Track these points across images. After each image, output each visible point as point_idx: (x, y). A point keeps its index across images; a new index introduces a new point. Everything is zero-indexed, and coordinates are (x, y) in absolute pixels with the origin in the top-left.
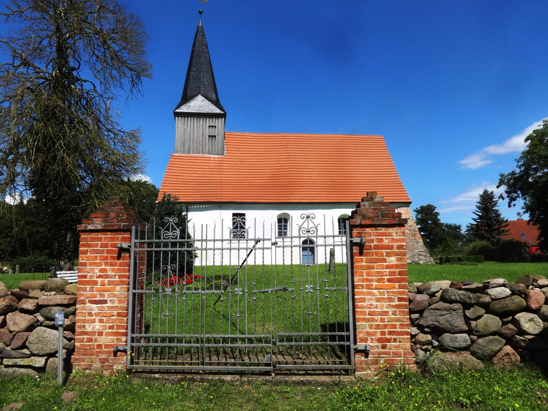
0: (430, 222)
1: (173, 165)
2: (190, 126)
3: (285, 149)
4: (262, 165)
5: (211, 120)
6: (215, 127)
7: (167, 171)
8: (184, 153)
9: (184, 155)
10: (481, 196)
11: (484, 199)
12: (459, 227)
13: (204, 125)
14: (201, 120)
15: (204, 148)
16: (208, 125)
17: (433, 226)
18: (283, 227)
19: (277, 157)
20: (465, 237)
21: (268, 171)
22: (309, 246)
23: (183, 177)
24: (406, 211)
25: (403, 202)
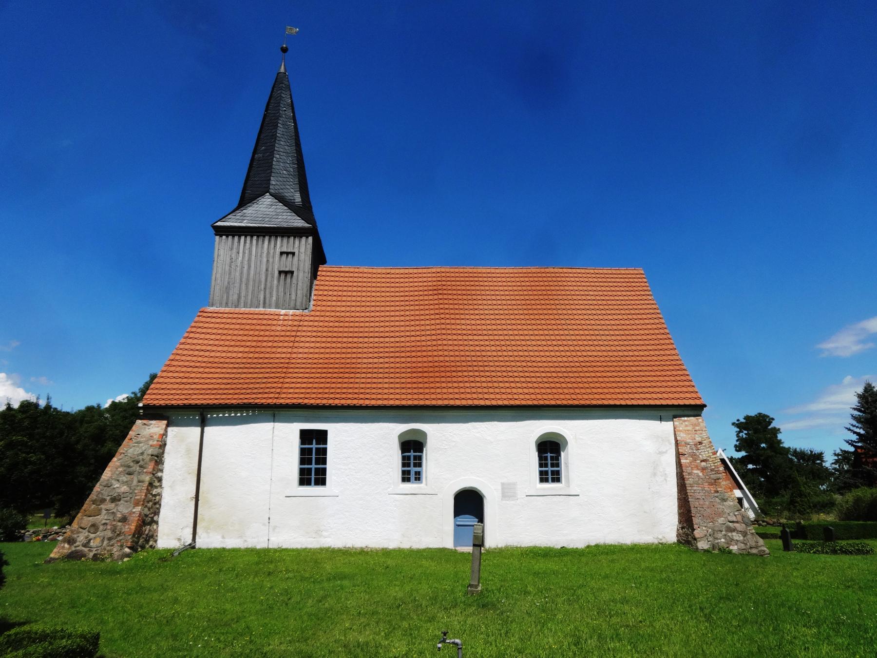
0: (763, 445)
1: (199, 330)
2: (244, 253)
3: (436, 297)
4: (382, 329)
5: (285, 240)
6: (293, 254)
7: (183, 340)
8: (227, 305)
9: (227, 310)
10: (859, 396)
11: (867, 403)
12: (820, 456)
13: (272, 251)
14: (254, 241)
15: (268, 296)
16: (278, 251)
17: (769, 452)
18: (412, 461)
19: (417, 313)
20: (832, 474)
21: (392, 340)
22: (469, 503)
23: (213, 354)
24: (695, 425)
25: (685, 406)
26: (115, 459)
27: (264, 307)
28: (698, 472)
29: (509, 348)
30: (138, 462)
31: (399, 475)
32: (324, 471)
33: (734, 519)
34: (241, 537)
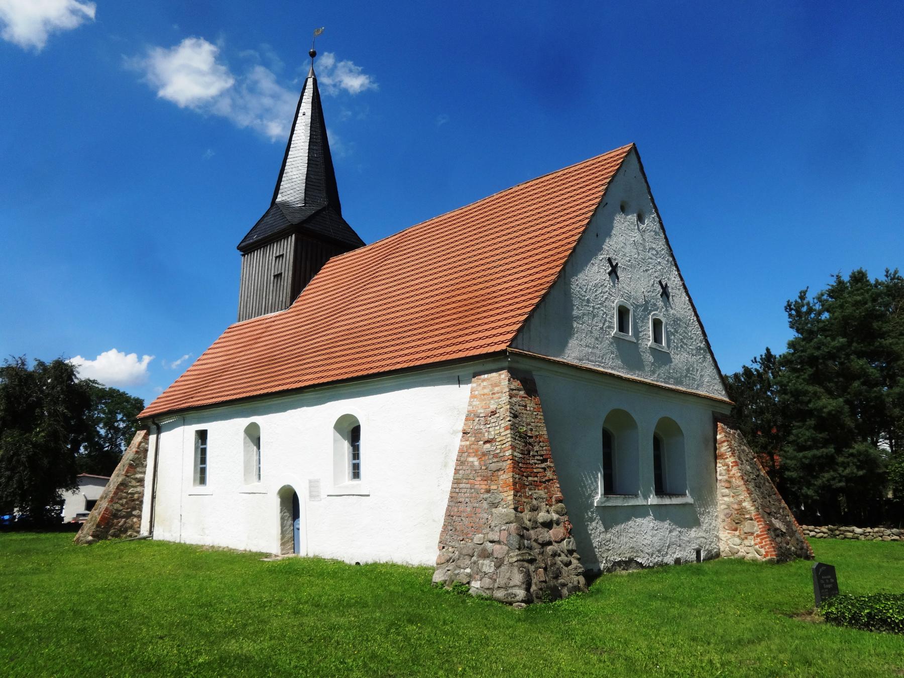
22: (290, 503)
31: (351, 475)
33: (496, 538)
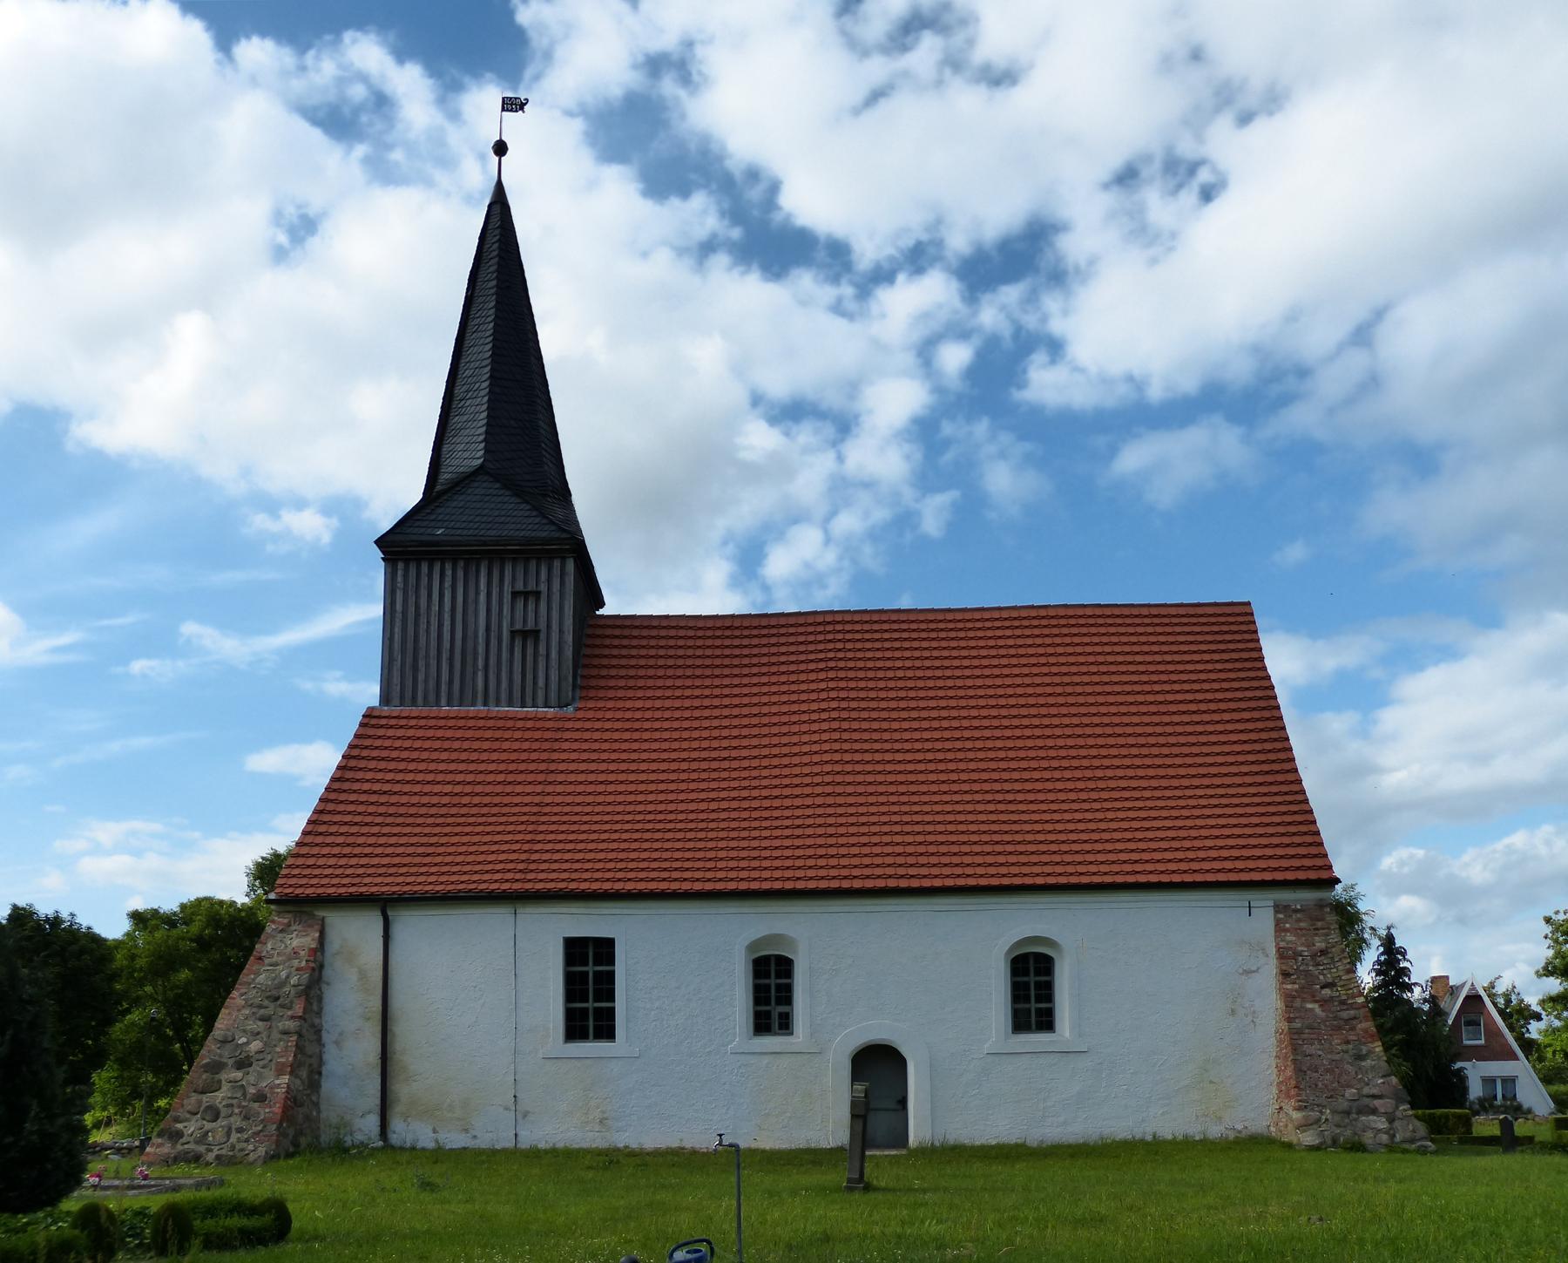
8: (414, 703)
22: (772, 991)
23: (394, 799)
26: (235, 994)
27: (485, 704)
28: (1315, 1006)
29: (964, 776)
30: (277, 999)
32: (610, 1014)
34: (466, 1131)
